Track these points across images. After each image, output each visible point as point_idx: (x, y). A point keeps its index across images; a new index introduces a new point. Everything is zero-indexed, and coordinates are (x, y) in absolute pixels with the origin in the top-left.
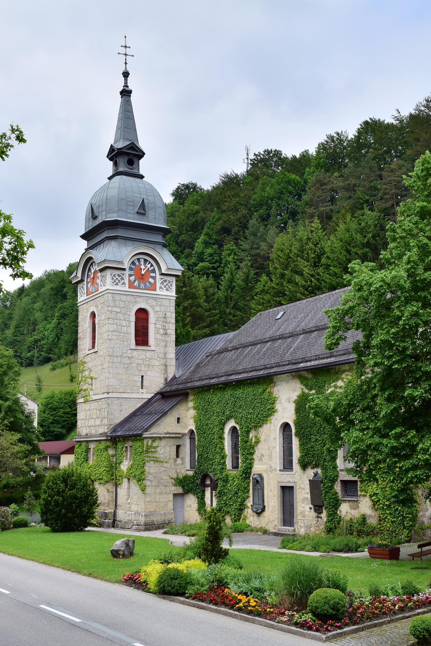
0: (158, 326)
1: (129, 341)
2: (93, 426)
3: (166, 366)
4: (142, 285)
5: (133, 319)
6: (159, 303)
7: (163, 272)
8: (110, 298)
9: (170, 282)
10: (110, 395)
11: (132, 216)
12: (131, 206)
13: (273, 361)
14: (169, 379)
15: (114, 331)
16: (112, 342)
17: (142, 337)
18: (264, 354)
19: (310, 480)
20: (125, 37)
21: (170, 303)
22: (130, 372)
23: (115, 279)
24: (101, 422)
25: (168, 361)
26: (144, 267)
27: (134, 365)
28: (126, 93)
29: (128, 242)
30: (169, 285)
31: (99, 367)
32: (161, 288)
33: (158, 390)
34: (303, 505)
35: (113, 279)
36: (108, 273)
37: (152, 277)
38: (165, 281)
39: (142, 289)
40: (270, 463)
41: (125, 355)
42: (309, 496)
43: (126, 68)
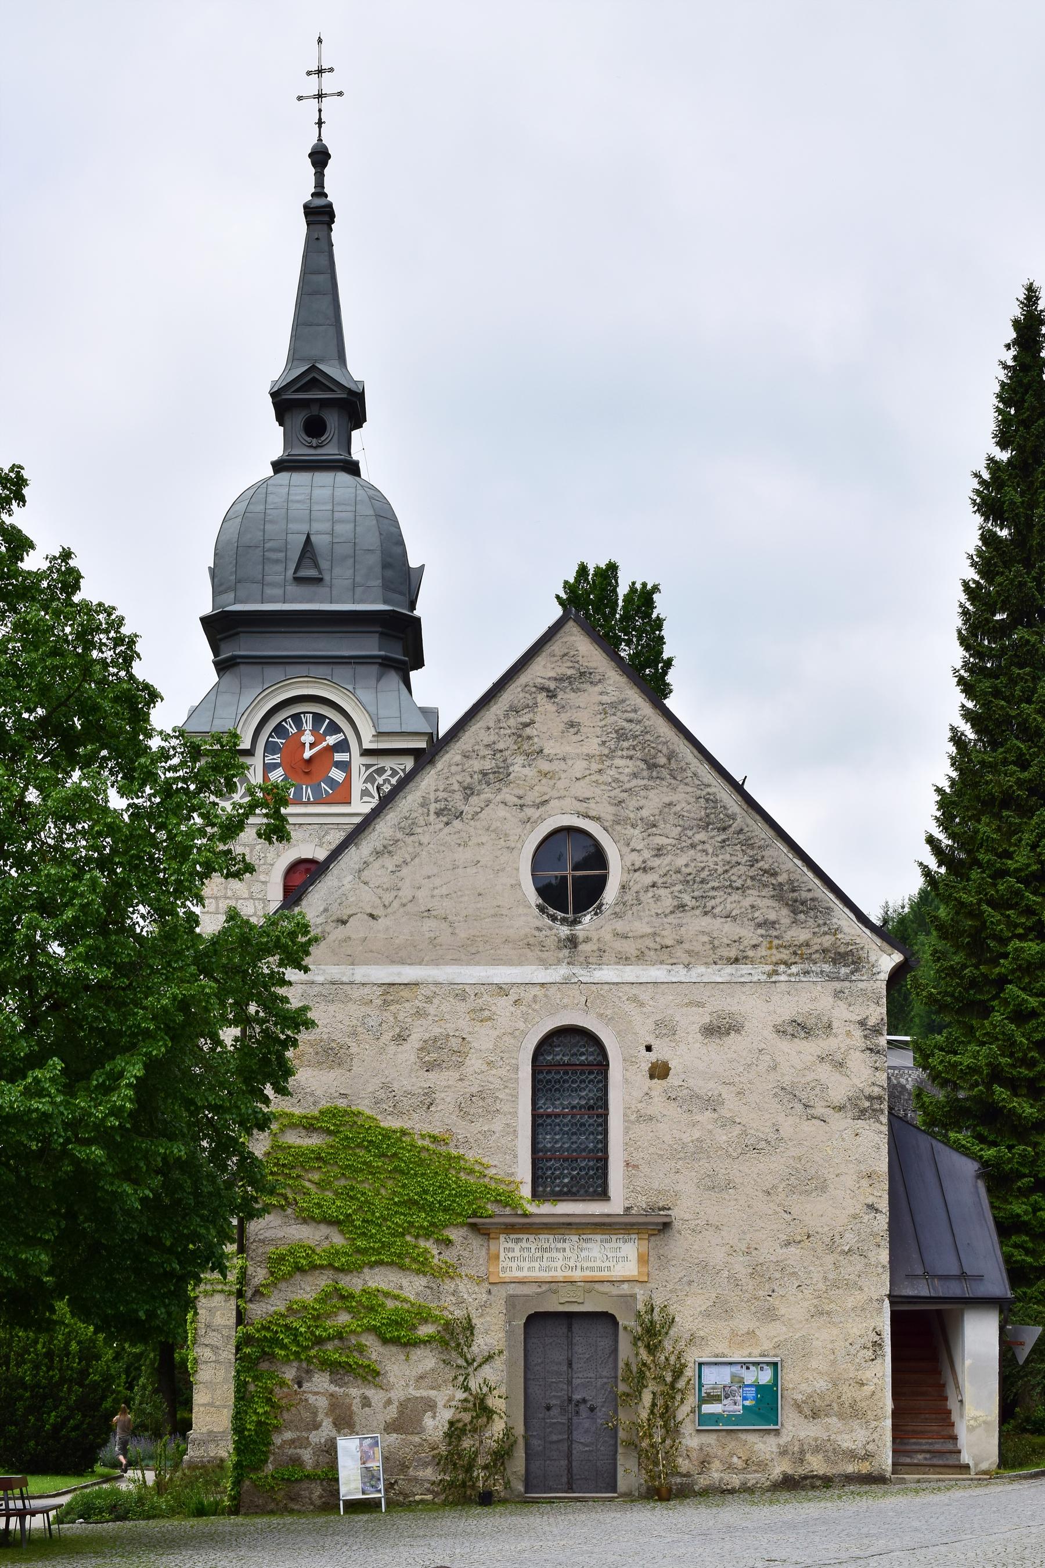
11: (279, 592)
12: (277, 561)
20: (320, 41)
26: (312, 739)
28: (320, 215)
29: (293, 670)
37: (339, 765)
38: (381, 771)
39: (308, 803)
43: (320, 140)
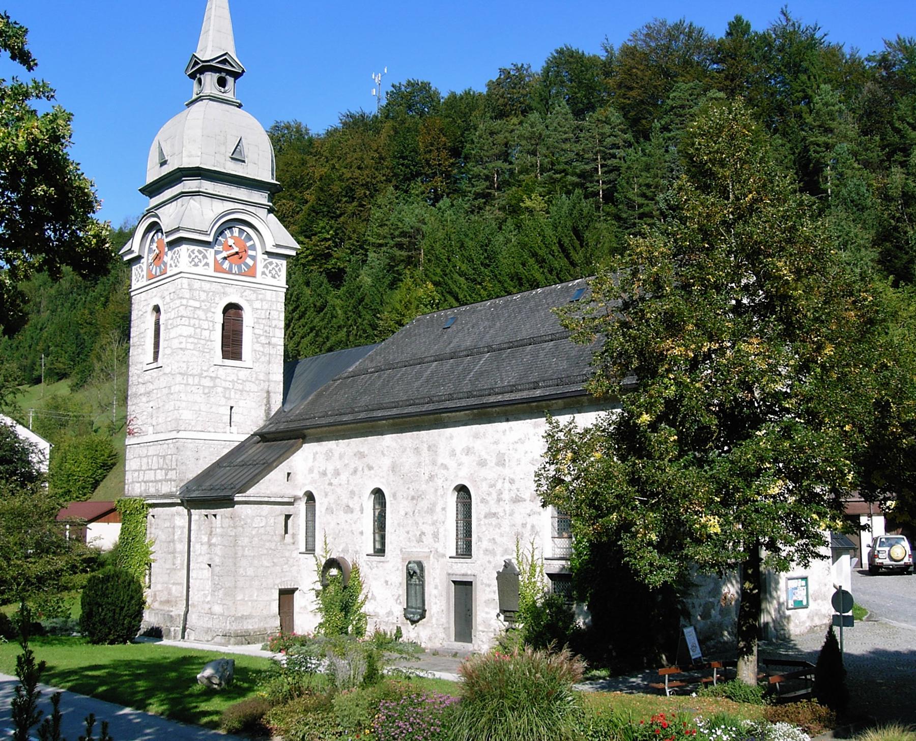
0: (257, 331)
1: (212, 352)
2: (152, 482)
3: (268, 392)
4: (235, 269)
5: (220, 318)
6: (260, 296)
7: (268, 250)
8: (185, 286)
9: (277, 265)
10: (182, 435)
13: (442, 391)
14: (273, 413)
15: (190, 336)
16: (187, 352)
17: (232, 345)
18: (427, 381)
19: (498, 573)
21: (277, 296)
22: (212, 400)
23: (193, 256)
24: (166, 475)
25: (272, 385)
27: (220, 390)
30: (277, 269)
31: (165, 391)
32: (263, 273)
33: (255, 429)
34: (487, 610)
35: (190, 256)
36: (184, 248)
38: (271, 263)
39: (235, 274)
40: (436, 545)
41: (205, 374)
42: (496, 597)
